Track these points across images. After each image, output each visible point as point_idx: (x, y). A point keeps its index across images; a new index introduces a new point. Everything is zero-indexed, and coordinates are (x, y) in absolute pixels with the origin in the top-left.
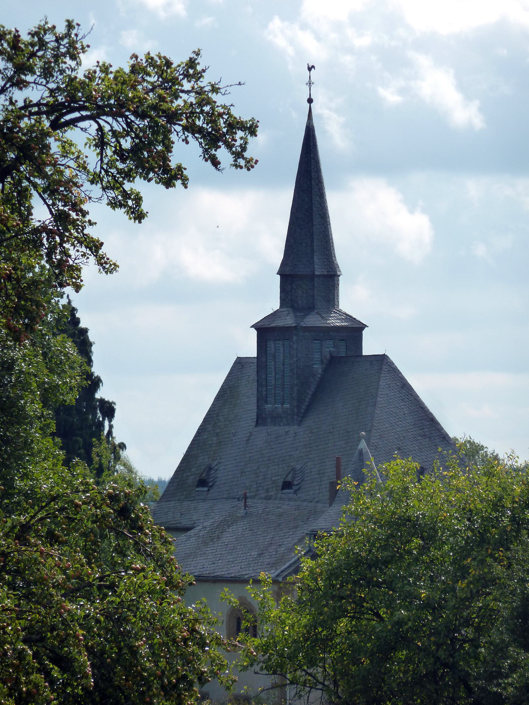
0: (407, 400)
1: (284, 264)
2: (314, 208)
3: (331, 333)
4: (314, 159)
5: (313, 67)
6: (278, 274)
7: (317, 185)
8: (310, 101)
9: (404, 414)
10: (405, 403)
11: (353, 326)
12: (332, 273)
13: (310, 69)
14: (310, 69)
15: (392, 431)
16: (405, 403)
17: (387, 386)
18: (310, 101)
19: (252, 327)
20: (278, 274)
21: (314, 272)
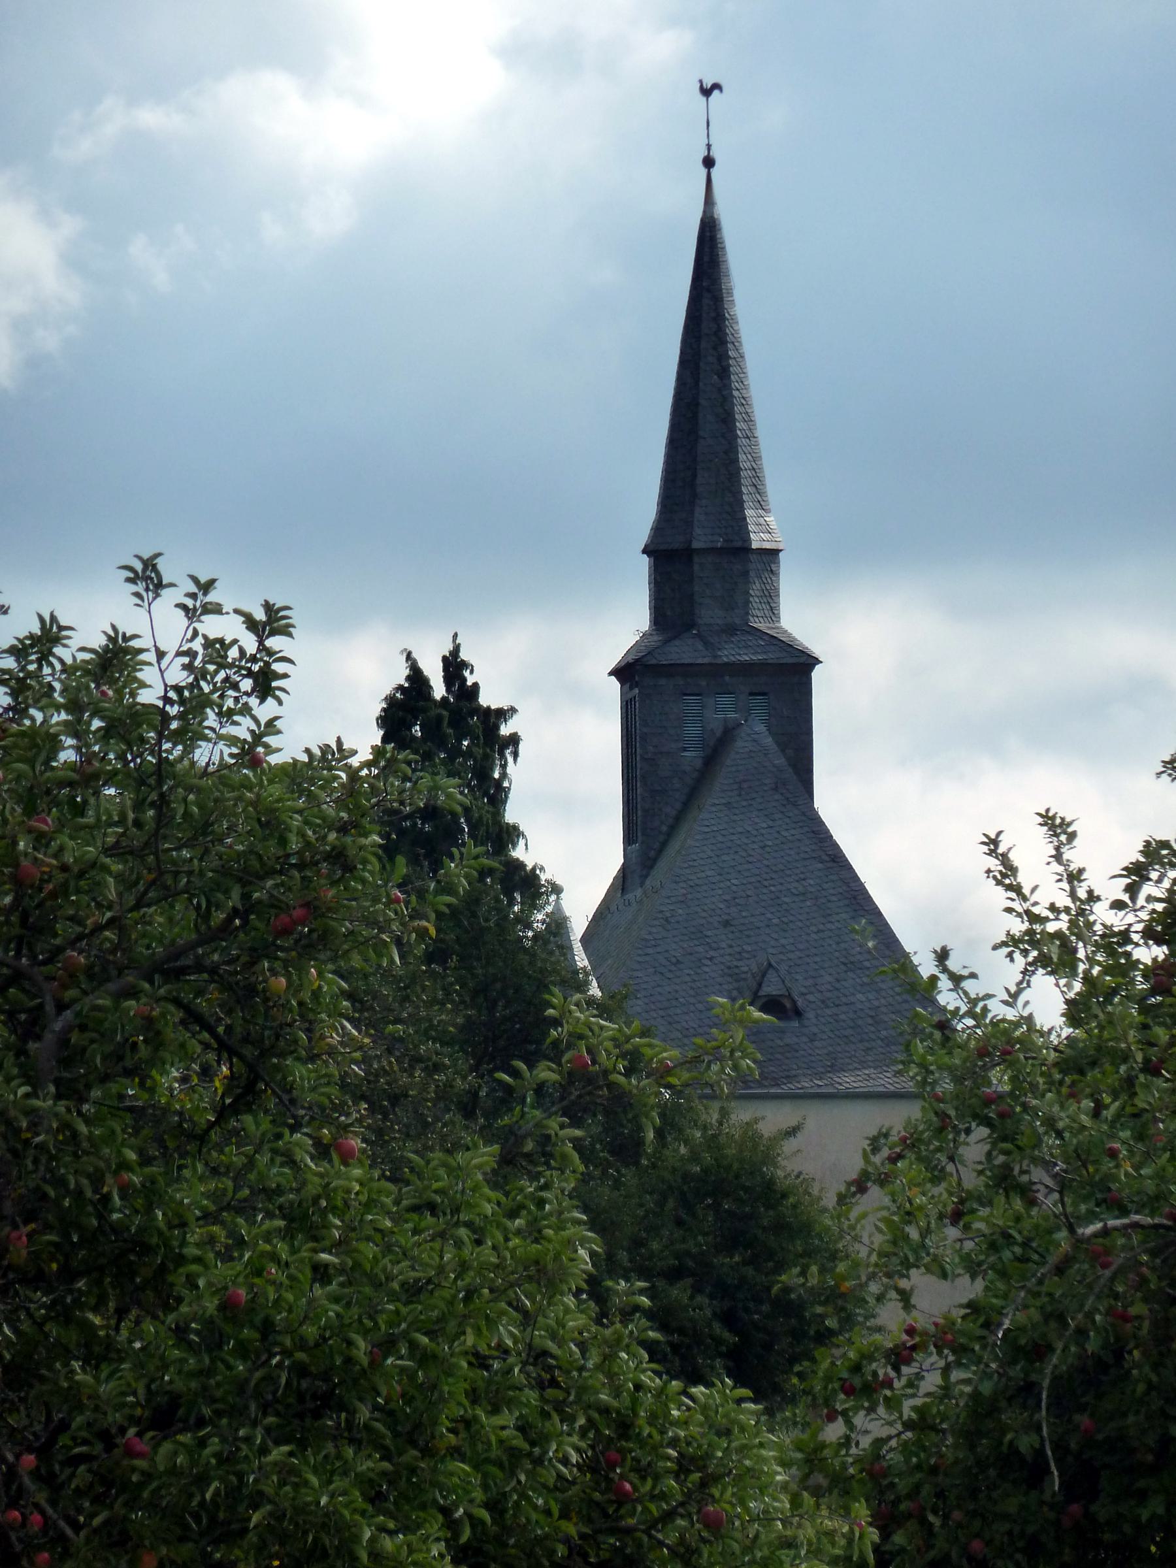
0: (780, 816)
1: (659, 529)
2: (702, 402)
3: (727, 678)
4: (709, 291)
5: (717, 86)
6: (644, 552)
7: (715, 348)
8: (709, 162)
9: (763, 848)
10: (771, 823)
11: (784, 661)
12: (739, 544)
13: (706, 92)
14: (706, 92)
15: (722, 885)
16: (771, 823)
17: (736, 786)
18: (709, 162)
19: (611, 674)
20: (644, 552)
21: (691, 541)
